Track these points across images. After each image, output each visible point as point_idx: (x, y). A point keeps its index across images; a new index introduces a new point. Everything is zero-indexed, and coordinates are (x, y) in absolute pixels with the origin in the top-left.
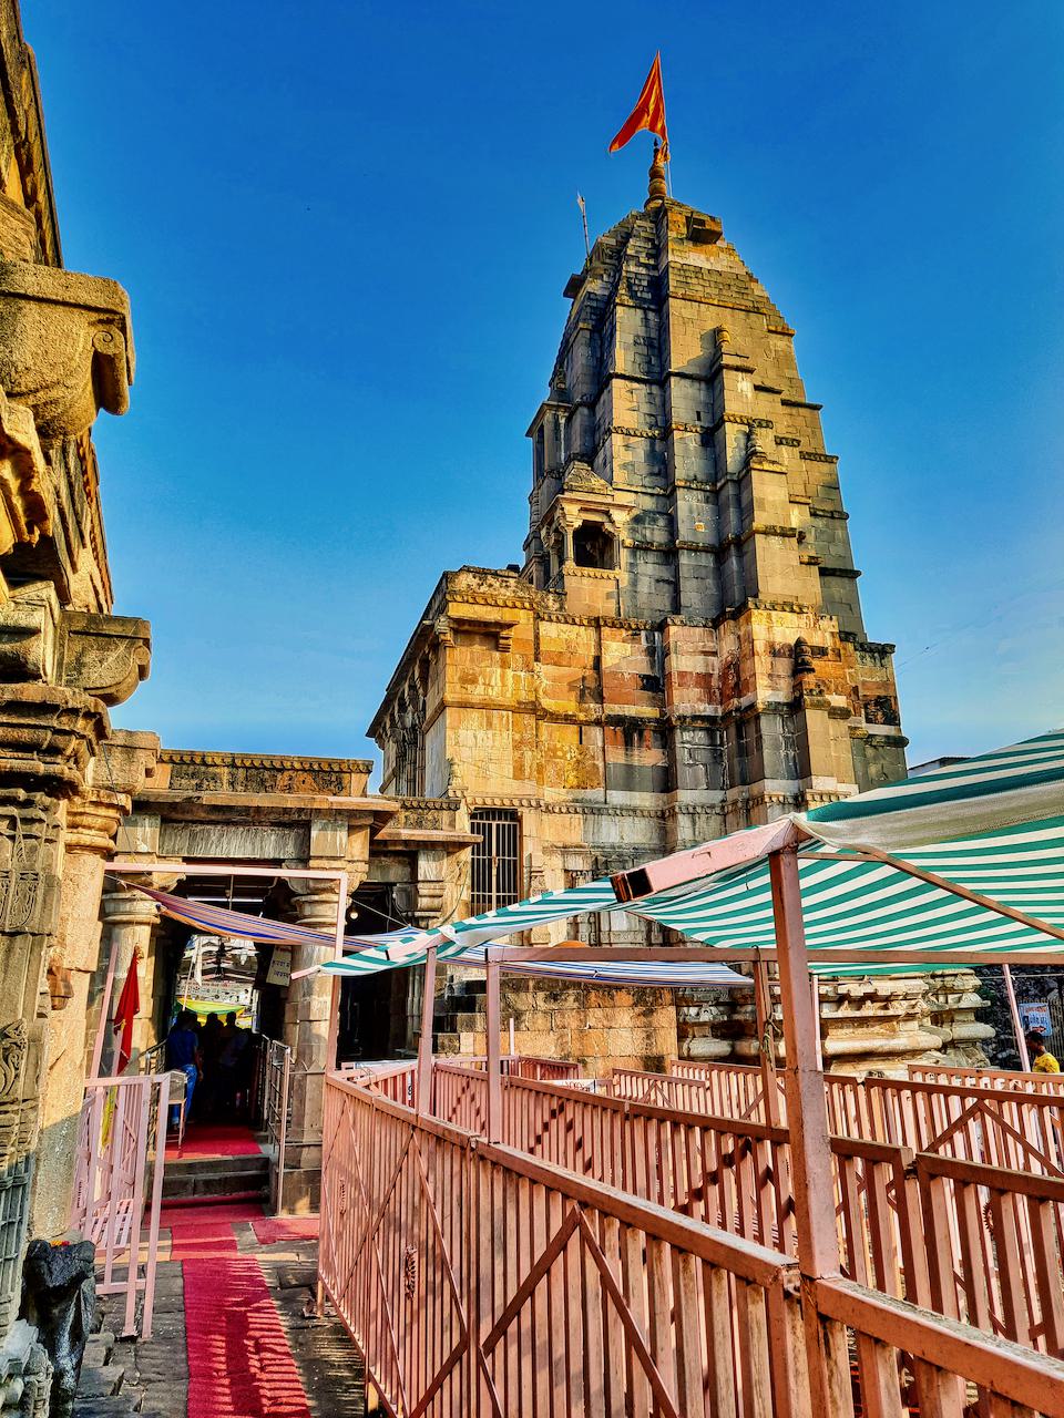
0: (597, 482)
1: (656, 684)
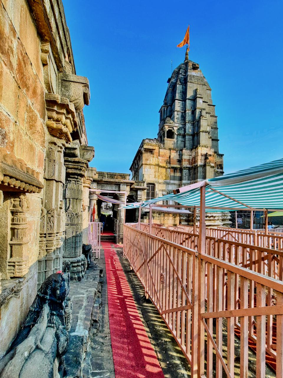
0: (171, 121)
1: (180, 161)
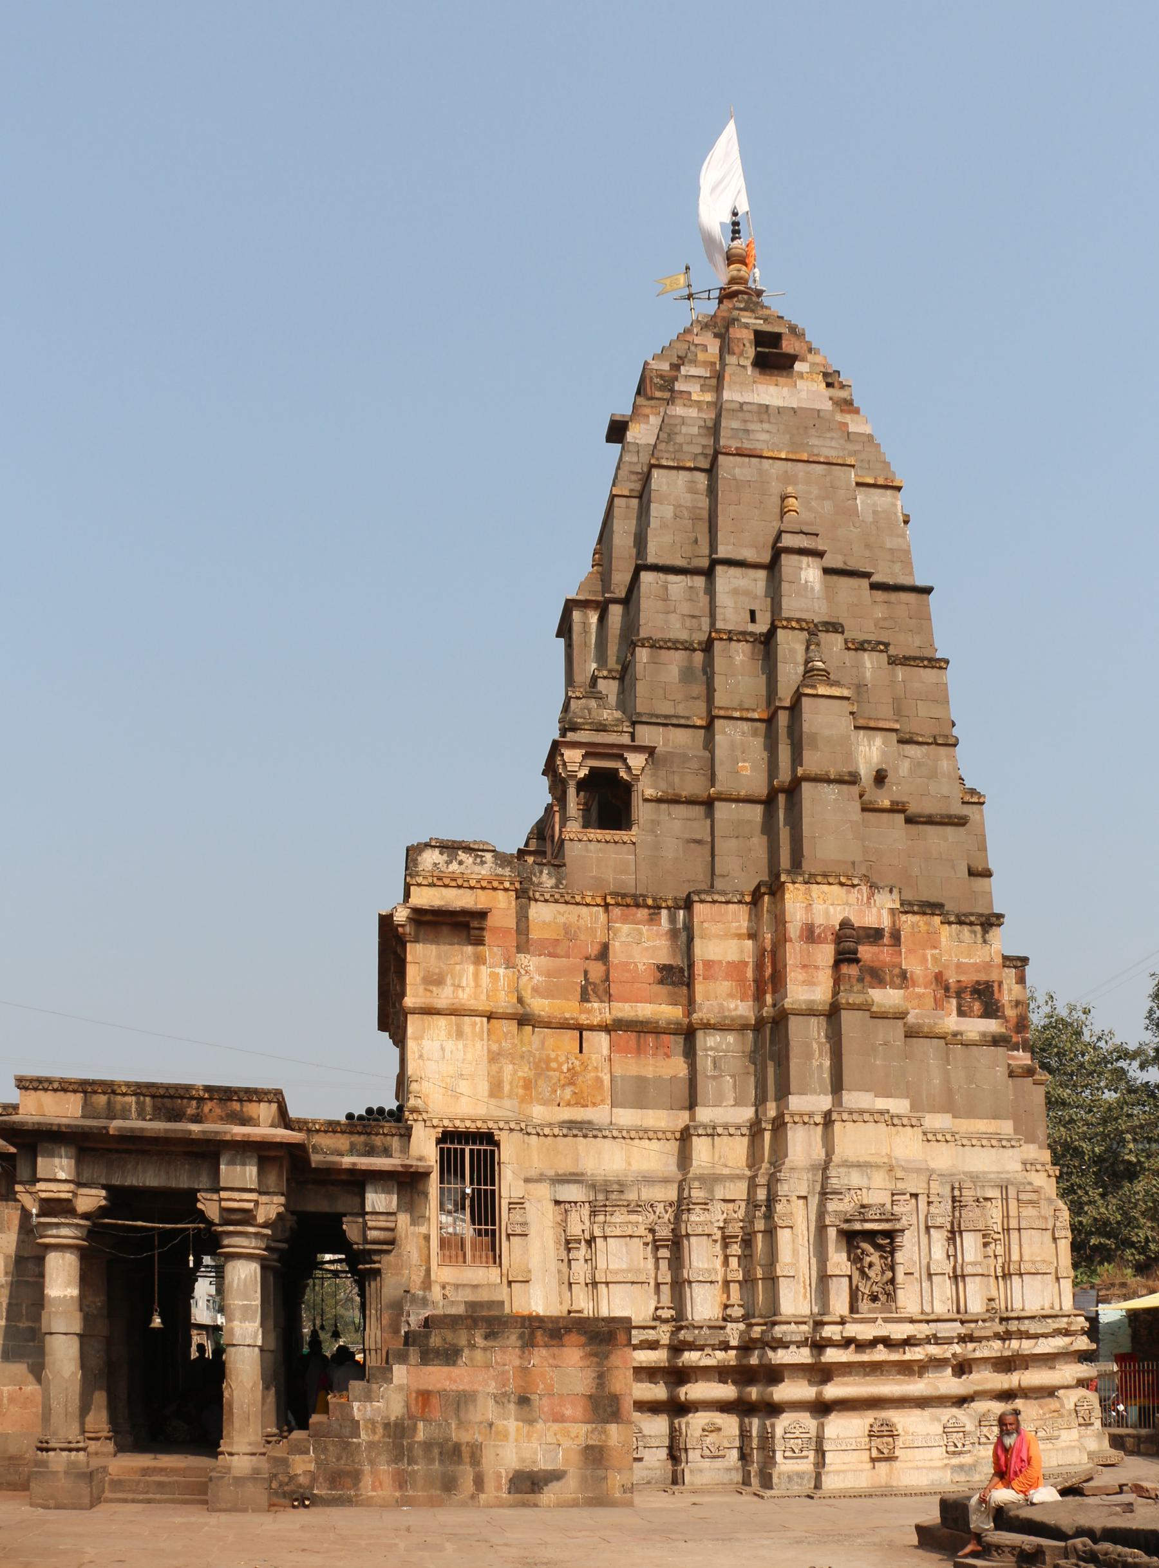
1: (678, 977)
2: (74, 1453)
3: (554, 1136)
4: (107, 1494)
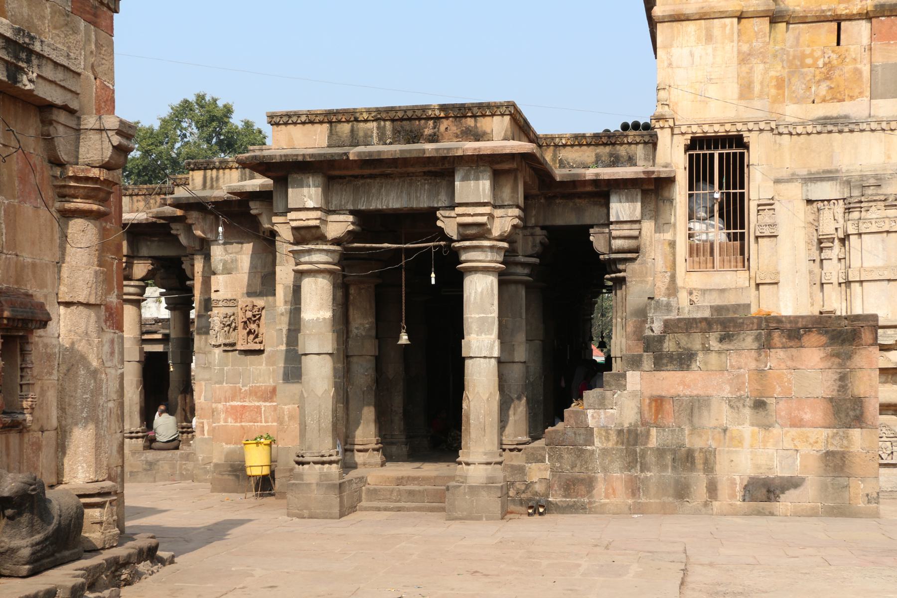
2: (327, 466)
3: (808, 134)
4: (364, 503)
